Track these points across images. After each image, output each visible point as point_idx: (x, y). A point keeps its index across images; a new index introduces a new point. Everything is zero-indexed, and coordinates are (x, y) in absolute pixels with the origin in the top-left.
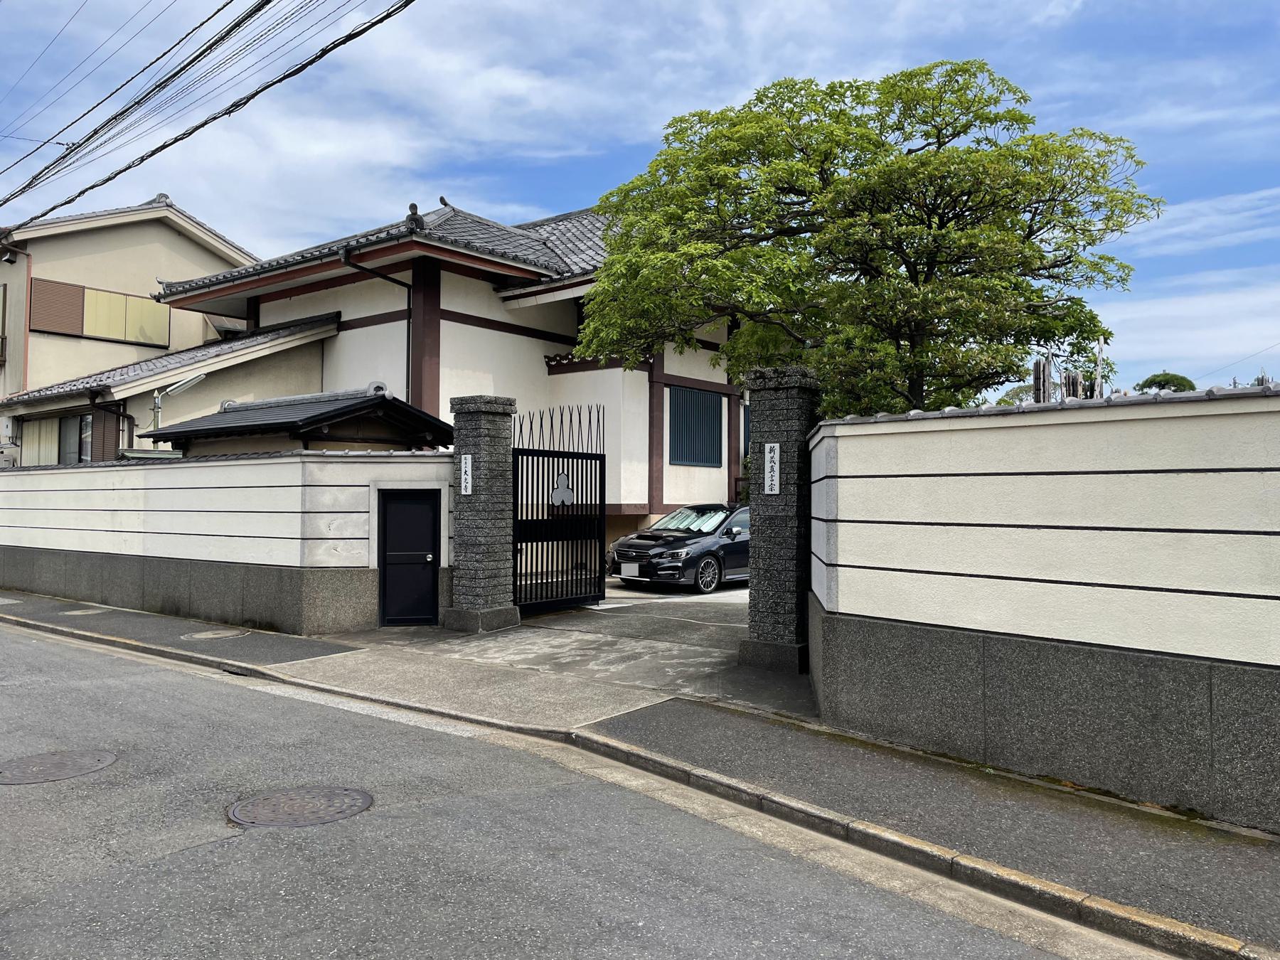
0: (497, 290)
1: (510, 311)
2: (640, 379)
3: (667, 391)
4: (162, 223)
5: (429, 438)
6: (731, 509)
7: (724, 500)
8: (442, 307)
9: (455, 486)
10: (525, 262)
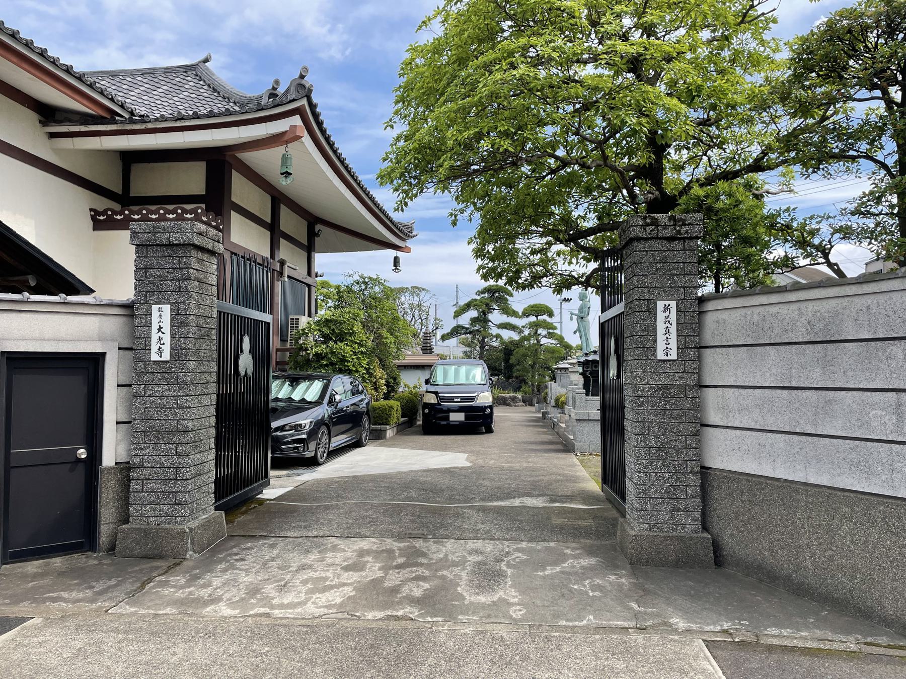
0: (44, 123)
1: (57, 151)
5: (33, 283)
9: (136, 345)
10: (102, 93)
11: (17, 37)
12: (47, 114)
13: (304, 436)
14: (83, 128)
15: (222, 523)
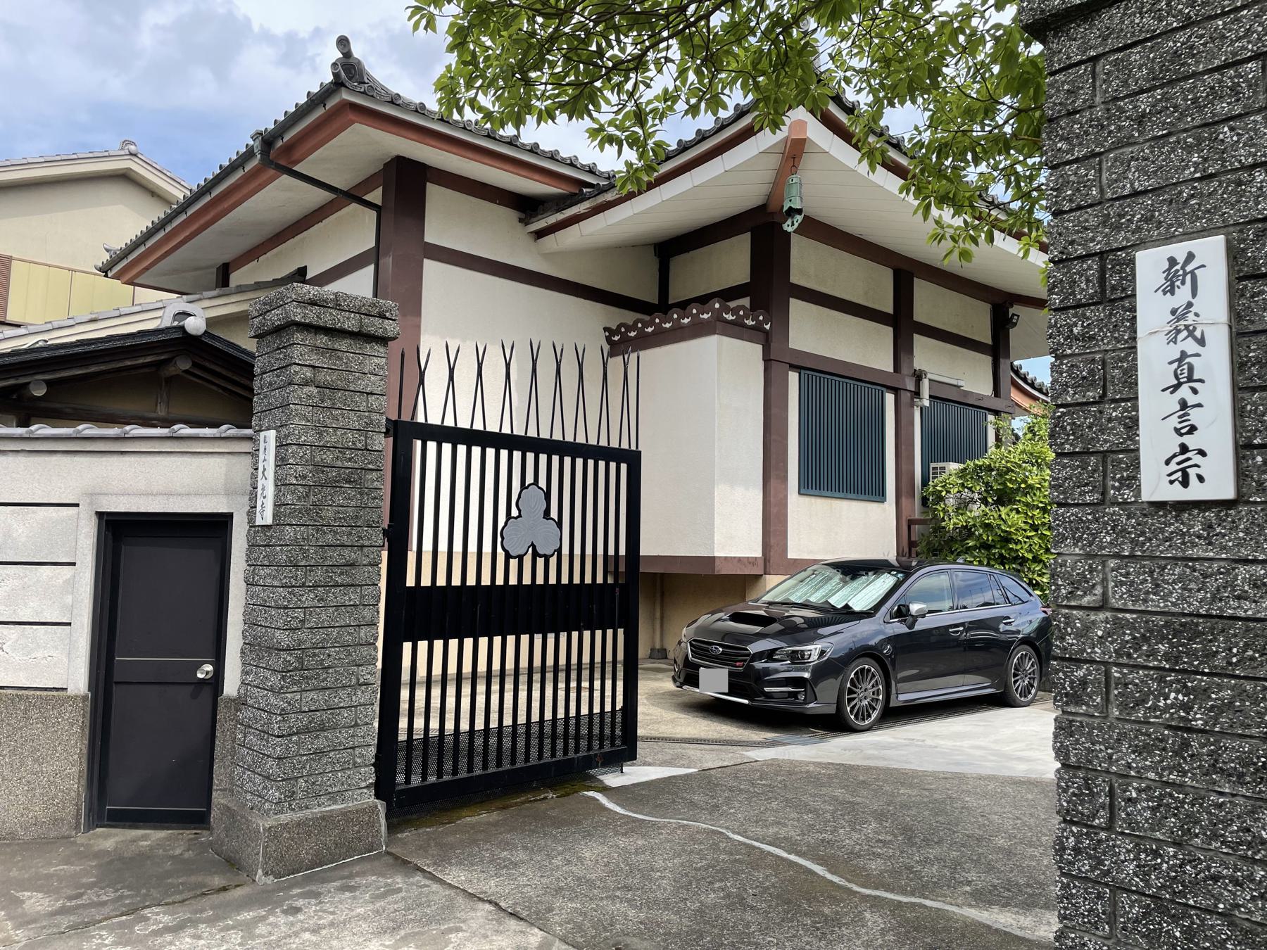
0: (525, 221)
1: (549, 256)
2: (754, 351)
3: (793, 377)
4: (125, 178)
6: (905, 570)
7: (887, 549)
8: (426, 240)
11: (400, 102)
12: (527, 206)
13: (807, 675)
14: (560, 217)
15: (372, 824)
